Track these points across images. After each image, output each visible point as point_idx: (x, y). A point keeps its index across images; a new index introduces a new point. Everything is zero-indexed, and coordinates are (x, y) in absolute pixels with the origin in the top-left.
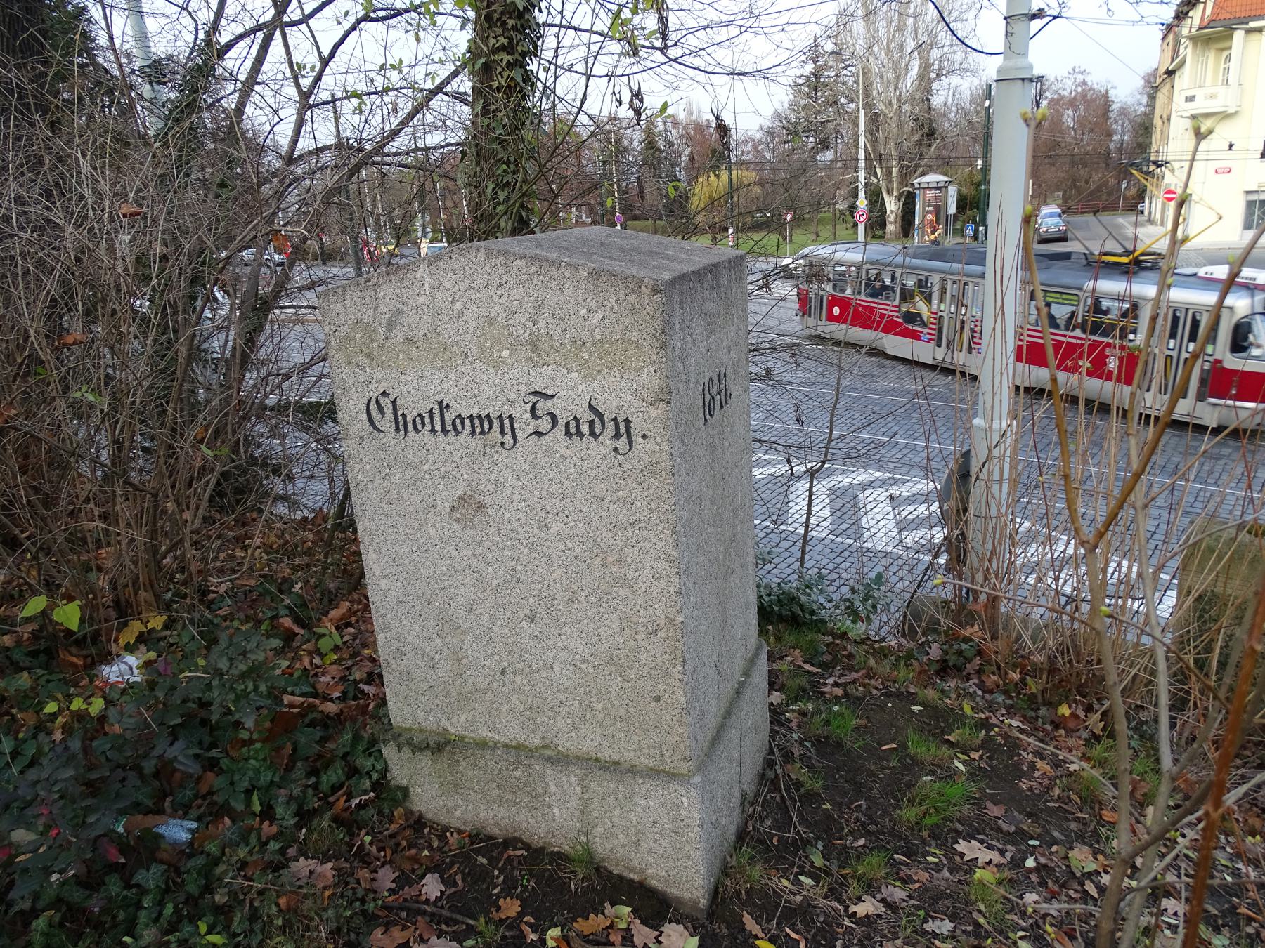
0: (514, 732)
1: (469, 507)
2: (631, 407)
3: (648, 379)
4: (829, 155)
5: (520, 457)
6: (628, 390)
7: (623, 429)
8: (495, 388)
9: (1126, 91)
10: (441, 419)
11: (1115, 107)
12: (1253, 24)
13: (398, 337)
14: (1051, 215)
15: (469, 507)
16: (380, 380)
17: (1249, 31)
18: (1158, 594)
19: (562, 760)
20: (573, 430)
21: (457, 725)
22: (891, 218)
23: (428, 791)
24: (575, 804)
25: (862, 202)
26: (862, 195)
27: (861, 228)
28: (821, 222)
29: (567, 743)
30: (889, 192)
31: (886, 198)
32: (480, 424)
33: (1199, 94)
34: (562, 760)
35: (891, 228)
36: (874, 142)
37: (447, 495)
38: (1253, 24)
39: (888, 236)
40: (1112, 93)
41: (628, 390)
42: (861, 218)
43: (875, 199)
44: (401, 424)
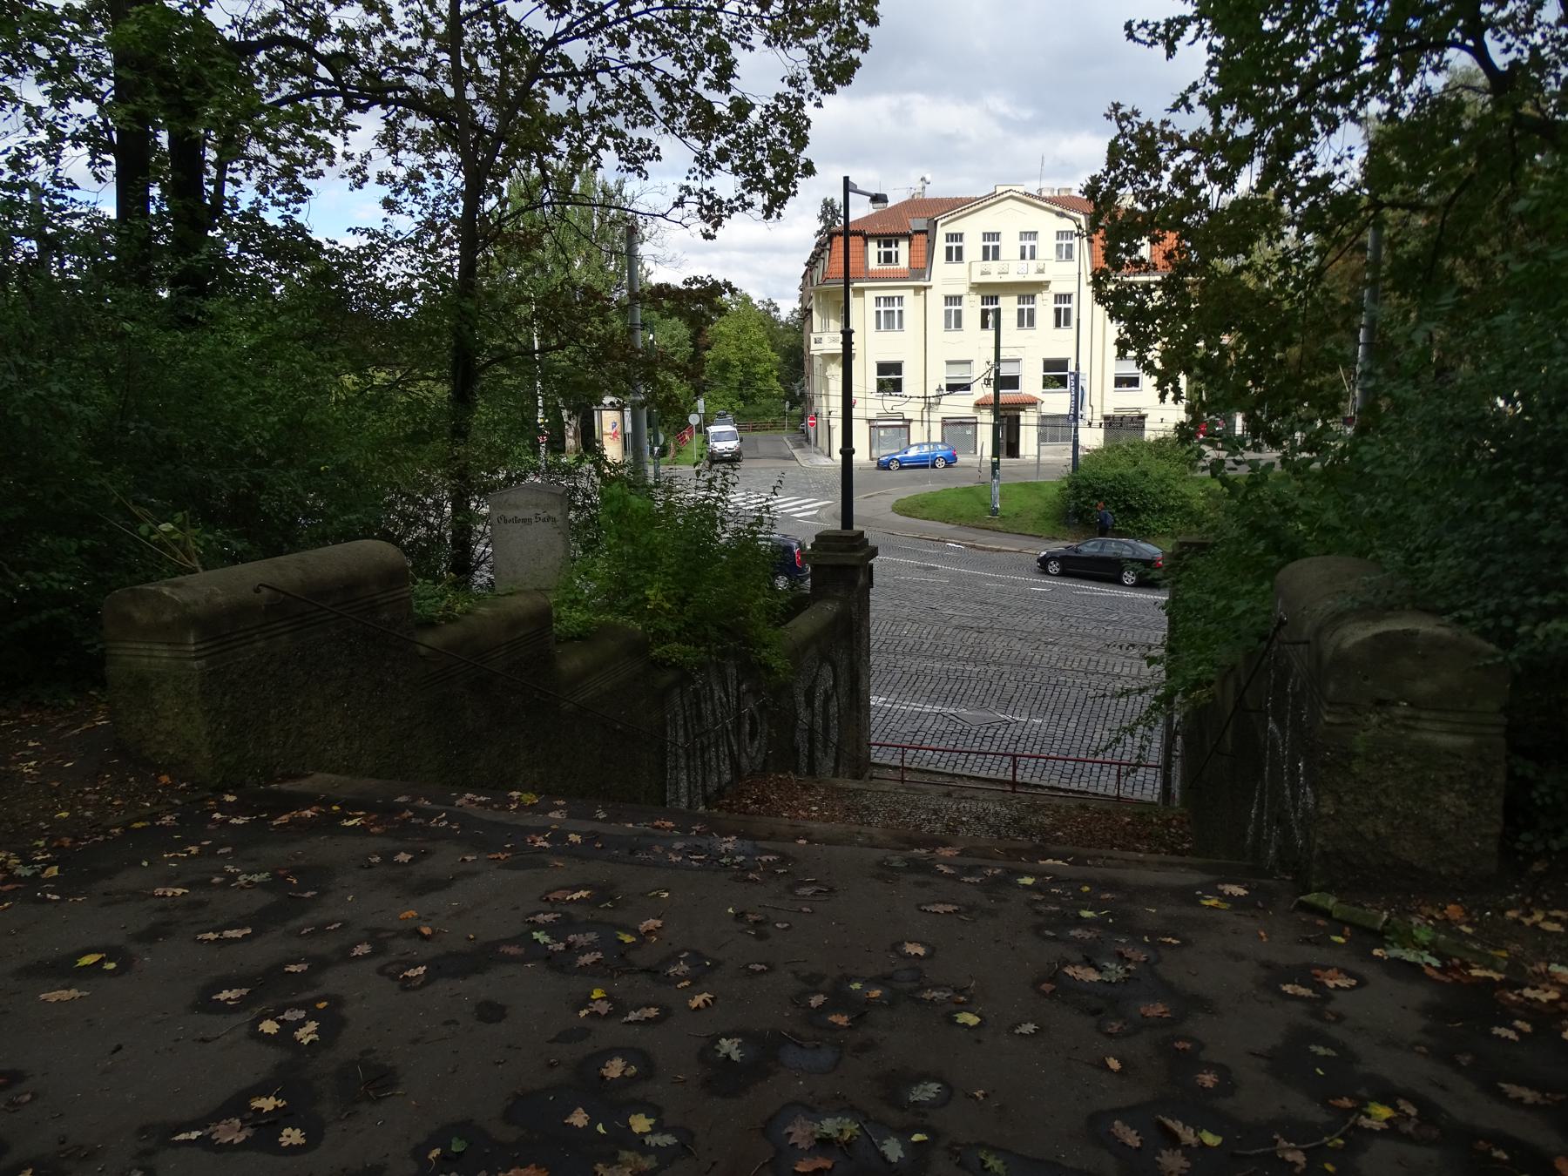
8: (529, 513)
9: (788, 307)
10: (516, 520)
16: (502, 512)
32: (524, 521)
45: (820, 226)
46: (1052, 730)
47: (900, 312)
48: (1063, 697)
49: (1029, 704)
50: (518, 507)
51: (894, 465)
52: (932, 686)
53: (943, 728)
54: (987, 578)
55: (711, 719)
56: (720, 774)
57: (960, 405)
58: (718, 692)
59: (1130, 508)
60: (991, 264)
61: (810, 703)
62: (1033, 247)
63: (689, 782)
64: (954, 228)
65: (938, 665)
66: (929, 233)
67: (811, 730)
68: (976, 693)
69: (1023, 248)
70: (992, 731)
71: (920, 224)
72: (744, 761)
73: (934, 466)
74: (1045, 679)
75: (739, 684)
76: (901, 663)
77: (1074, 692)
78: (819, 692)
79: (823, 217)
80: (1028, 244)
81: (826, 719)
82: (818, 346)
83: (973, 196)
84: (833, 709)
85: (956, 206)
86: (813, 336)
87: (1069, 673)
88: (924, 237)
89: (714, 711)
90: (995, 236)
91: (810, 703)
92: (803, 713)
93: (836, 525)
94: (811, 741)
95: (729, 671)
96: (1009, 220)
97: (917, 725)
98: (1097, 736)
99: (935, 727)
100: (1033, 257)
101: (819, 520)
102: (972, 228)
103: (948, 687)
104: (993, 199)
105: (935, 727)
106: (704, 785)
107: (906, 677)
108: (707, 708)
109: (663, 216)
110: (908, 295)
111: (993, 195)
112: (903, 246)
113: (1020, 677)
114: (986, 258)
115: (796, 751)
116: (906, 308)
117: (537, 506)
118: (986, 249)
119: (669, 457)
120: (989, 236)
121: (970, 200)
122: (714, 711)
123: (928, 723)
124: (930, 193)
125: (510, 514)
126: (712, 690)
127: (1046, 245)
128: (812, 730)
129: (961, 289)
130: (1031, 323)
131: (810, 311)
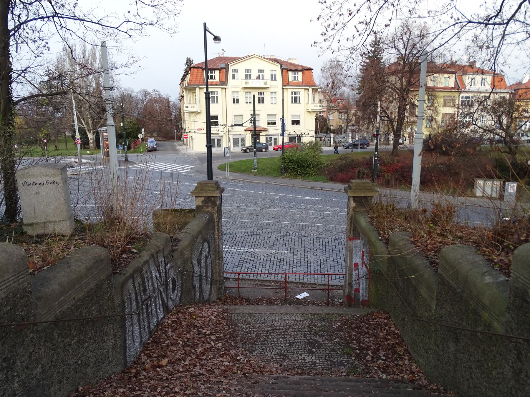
0: (43, 220)
1: (37, 193)
2: (58, 180)
3: (60, 178)
4: (60, 115)
5: (44, 187)
6: (58, 179)
7: (57, 183)
8: (42, 180)
9: (174, 98)
10: (34, 184)
11: (172, 103)
12: (200, 87)
13: (28, 175)
14: (151, 142)
15: (37, 193)
16: (24, 180)
17: (200, 89)
18: (264, 315)
19: (50, 222)
20: (51, 183)
21: (35, 221)
22: (91, 141)
23: (30, 231)
24: (52, 227)
25: (78, 136)
26: (77, 131)
27: (79, 146)
28: (59, 141)
29: (51, 220)
30: (89, 131)
31: (88, 133)
32: (39, 184)
33: (189, 106)
34: (50, 222)
35: (91, 145)
36: (80, 112)
37: (34, 192)
38: (200, 87)
39: (91, 148)
40: (170, 99)
41: (58, 179)
42: (78, 142)
43: (83, 133)
44: (28, 185)
45: (186, 67)
46: (292, 256)
47: (217, 97)
48: (293, 241)
49: (281, 245)
50: (34, 176)
51: (248, 151)
52: (242, 239)
53: (249, 258)
54: (256, 194)
55: (151, 289)
56: (157, 316)
57: (239, 131)
58: (155, 273)
59: (303, 166)
60: (248, 80)
61: (199, 263)
62: (263, 75)
63: (140, 328)
64: (235, 67)
65: (243, 230)
66: (226, 68)
67: (200, 276)
68: (260, 242)
69: (259, 75)
70: (269, 258)
71: (223, 65)
72: (170, 303)
73: (262, 151)
74: (285, 234)
75: (166, 265)
76: (229, 230)
77: (297, 238)
78: (203, 258)
79: (186, 64)
80: (261, 74)
81: (206, 268)
82: (187, 109)
83: (241, 56)
84: (209, 262)
85: (234, 59)
86: (185, 105)
87: (293, 230)
88: (224, 70)
89: (153, 284)
90: (250, 71)
91: (199, 263)
92: (197, 269)
93: (205, 177)
94: (201, 280)
95: (160, 260)
96: (254, 65)
97: (239, 257)
98: (309, 257)
99: (246, 258)
100: (263, 79)
101: (191, 173)
102: (241, 67)
103: (249, 240)
104: (248, 57)
105: (246, 258)
106: (149, 326)
107: (232, 236)
108: (148, 285)
109: (116, 28)
110: (219, 91)
111: (249, 56)
112: (217, 72)
113: (275, 233)
114: (246, 78)
115: (194, 287)
116: (219, 95)
117: (47, 175)
118: (246, 75)
119: (132, 150)
120: (247, 71)
121: (240, 58)
122: (153, 284)
123: (243, 256)
124: (226, 55)
125: (30, 181)
126: (151, 273)
127: (267, 75)
128: (200, 276)
129: (239, 89)
130: (263, 102)
131: (183, 97)
